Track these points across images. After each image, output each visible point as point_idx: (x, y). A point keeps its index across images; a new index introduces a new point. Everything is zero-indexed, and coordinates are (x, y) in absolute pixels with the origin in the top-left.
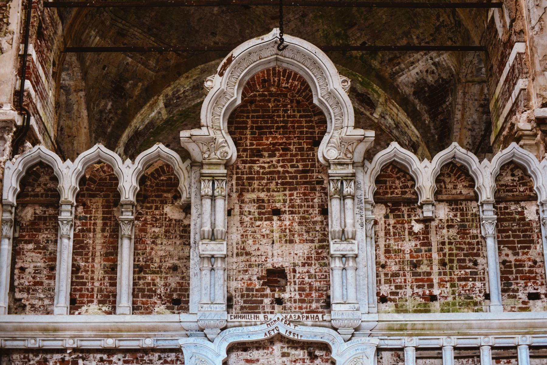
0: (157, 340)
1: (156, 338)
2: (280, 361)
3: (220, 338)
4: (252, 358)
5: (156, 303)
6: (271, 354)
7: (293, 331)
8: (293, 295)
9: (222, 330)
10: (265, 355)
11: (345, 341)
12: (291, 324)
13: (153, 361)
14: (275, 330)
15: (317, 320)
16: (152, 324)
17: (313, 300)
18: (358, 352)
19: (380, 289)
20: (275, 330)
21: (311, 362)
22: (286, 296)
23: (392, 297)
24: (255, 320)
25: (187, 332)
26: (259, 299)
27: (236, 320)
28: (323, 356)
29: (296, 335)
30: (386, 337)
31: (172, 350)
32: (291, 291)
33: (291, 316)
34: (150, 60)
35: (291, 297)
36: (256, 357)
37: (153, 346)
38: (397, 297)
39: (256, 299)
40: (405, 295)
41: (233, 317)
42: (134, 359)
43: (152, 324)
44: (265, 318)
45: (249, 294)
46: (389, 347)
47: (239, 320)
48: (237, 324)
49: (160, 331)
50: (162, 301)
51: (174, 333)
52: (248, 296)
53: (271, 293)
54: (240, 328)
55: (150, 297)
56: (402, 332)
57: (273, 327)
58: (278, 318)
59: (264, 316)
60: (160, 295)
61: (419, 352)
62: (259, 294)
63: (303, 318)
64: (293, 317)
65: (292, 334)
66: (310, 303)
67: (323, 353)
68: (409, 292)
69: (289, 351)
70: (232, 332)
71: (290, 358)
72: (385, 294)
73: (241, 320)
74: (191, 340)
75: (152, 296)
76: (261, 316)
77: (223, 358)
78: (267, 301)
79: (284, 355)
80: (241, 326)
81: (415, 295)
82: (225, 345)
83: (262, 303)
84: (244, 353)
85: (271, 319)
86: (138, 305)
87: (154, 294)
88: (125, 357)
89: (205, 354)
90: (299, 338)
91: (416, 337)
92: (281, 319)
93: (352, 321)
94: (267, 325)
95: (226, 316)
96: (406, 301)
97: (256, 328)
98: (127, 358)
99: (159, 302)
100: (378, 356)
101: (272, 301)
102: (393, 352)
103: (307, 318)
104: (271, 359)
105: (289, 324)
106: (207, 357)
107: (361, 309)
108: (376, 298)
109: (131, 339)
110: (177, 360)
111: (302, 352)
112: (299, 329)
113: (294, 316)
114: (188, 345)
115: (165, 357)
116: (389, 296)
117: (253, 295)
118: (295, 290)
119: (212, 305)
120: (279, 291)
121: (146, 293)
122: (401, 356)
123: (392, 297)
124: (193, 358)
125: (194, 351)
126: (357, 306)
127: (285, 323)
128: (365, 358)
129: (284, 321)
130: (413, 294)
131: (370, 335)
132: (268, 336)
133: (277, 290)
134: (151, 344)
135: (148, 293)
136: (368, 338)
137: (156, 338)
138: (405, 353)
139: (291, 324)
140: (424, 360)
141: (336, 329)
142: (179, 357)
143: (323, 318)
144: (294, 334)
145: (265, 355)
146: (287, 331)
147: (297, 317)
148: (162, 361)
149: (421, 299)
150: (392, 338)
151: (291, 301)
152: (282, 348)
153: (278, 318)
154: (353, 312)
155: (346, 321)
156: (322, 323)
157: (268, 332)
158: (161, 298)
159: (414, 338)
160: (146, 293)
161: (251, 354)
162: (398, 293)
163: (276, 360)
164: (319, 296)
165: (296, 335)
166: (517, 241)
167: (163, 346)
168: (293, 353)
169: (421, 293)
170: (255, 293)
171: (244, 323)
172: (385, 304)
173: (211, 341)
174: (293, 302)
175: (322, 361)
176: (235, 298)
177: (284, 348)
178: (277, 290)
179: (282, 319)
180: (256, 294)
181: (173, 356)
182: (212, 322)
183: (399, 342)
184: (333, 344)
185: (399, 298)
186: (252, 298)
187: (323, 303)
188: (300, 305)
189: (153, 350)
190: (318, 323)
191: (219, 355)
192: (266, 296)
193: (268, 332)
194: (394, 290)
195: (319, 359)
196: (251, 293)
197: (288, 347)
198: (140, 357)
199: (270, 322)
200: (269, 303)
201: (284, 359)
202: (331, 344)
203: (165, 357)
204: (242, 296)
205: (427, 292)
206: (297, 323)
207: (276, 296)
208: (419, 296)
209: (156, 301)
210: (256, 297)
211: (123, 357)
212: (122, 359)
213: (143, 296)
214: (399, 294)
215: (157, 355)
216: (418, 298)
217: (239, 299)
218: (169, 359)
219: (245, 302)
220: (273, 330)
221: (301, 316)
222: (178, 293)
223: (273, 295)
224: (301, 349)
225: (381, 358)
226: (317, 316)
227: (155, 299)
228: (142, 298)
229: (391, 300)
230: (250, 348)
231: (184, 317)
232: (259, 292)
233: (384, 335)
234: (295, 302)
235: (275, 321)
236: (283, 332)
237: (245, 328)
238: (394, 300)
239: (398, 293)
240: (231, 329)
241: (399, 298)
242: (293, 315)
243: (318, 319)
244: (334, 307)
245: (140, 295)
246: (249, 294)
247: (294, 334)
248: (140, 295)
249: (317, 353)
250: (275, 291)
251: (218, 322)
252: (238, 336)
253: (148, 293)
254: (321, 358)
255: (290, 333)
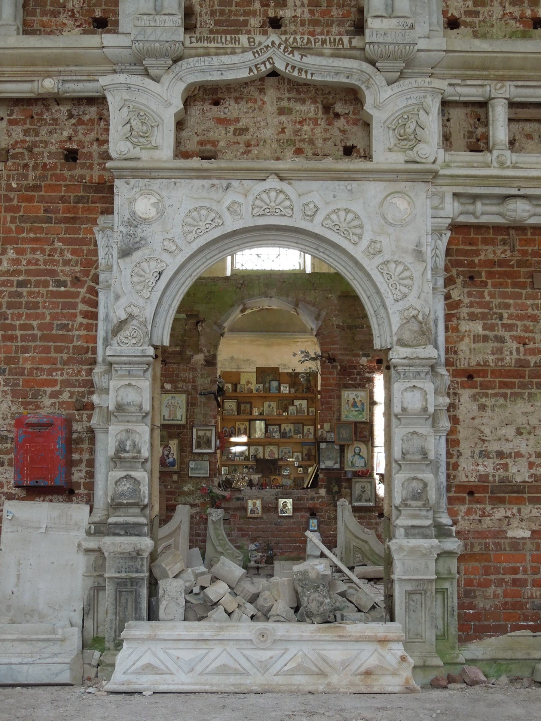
0: (64, 81)
1: (61, 78)
2: (276, 121)
3: (171, 75)
4: (229, 116)
5: (65, 24)
6: (260, 109)
7: (297, 64)
8: (299, 12)
9: (175, 61)
10: (251, 111)
11: (390, 83)
12: (296, 53)
13: (60, 121)
14: (267, 63)
15: (340, 46)
16: (54, 51)
17: (333, 22)
18: (410, 102)
19: (448, 6)
20: (267, 63)
21: (329, 124)
22: (287, 13)
23: (468, 19)
24: (234, 46)
25: (115, 67)
26: (241, 18)
27: (199, 45)
28: (348, 114)
29: (303, 73)
30: (459, 82)
31: (91, 101)
32: (295, 6)
33: (295, 39)
34: (251, 391)
35: (295, 16)
36: (235, 115)
37: (56, 90)
38: (476, 20)
39: (235, 18)
40: (491, 16)
41: (194, 40)
42: (26, 117)
43: (54, 51)
44: (249, 42)
45: (224, 10)
46: (462, 99)
47: (206, 44)
48: (201, 51)
49: (68, 65)
50: (76, 20)
51: (93, 68)
52: (222, 13)
53: (262, 9)
54: (206, 58)
55: (55, 14)
56: (486, 73)
57: (264, 57)
58: (273, 43)
59: (249, 39)
60: (72, 11)
61: (514, 110)
62: (241, 9)
63: (315, 43)
64: (299, 40)
65: (296, 69)
66: (328, 25)
67: (348, 109)
68: (497, 11)
69: (291, 105)
70: (192, 64)
71: (292, 117)
72: (456, 15)
73: (210, 45)
74: (122, 78)
75: (59, 13)
76: (244, 39)
77: (176, 110)
78: (254, 22)
79: (282, 111)
80: (208, 55)
81: (507, 17)
82: (181, 87)
83: (247, 26)
84: (215, 108)
85: (260, 44)
86: (35, 28)
87: (61, 10)
88: (11, 115)
89: (144, 101)
90: (309, 77)
91: (510, 83)
92: (277, 43)
93: (401, 47)
94: (254, 53)
95: (180, 35)
96: (492, 26)
97: (235, 59)
98: (14, 117)
99: (70, 22)
100: (443, 115)
101: (264, 21)
102: (469, 110)
103: (324, 42)
104: (259, 119)
105: (292, 52)
106: (148, 107)
107: (417, 28)
108: (442, 20)
109: (19, 79)
110: (101, 119)
111: (313, 108)
112: (310, 60)
113: (301, 40)
114: (117, 87)
115: (79, 115)
116: (463, 18)
117: (230, 11)
118: (303, 5)
119: (157, 17)
120: (275, 6)
121: (48, 8)
122: (483, 117)
123: (468, 19)
124: (125, 110)
125: (126, 97)
126: (410, 22)
127: (284, 51)
128: (422, 112)
129: (282, 47)
130: (504, 15)
131: (431, 75)
132: (256, 72)
133: (272, 4)
134: (53, 88)
135: (52, 8)
136: (429, 79)
137: (61, 78)
138: (490, 110)
139: (296, 53)
140: (521, 124)
141: (373, 63)
142: (103, 114)
143: (350, 42)
144: (300, 70)
145: (251, 111)
146: (287, 65)
147: (305, 41)
148: (73, 121)
149: (518, 24)
150: (469, 82)
151: (295, 22)
152: (280, 99)
153: (273, 43)
154: (403, 32)
155: (392, 47)
156: (349, 52)
157: (256, 66)
158: (73, 16)
159: (508, 83)
160: (48, 8)
161: (226, 110)
162: (479, 12)
163: (269, 120)
164: (344, 16)
165: (303, 73)
166: (512, 282)
167: (74, 91)
168: (298, 108)
169: (517, 14)
170: (233, 8)
171: (213, 51)
172: (455, 31)
173: (157, 79)
174: (298, 24)
175: (348, 122)
176: (201, 16)
177: (283, 99)
178: (272, 4)
179: (280, 45)
180: (237, 10)
181: (92, 112)
182: (157, 44)
183: (480, 91)
184: (368, 88)
185: (480, 22)
186: (229, 16)
187: (349, 26)
188: (312, 29)
189: (58, 100)
190: (342, 52)
191: (170, 104)
192: (254, 13)
193: (256, 66)
194: (471, 8)
195: (342, 118)
196: (227, 9)
197: (289, 99)
198: (38, 114)
199: (258, 49)
200: (258, 25)
201: (283, 118)
202: (363, 87)
203: (79, 115)
204: (213, 13)
205: (528, 13)
206: (305, 50)
207: (271, 14)
208: (515, 19)
209: (65, 21)
210: (236, 15)
211: (8, 115)
212: (6, 118)
213: (44, 13)
214: (481, 15)
215: (64, 109)
216: (512, 22)
217: (206, 18)
218: (86, 118)
219: (217, 23)
220: (264, 63)
221: (312, 39)
222: (103, 7)
223: (266, 12)
224: (311, 103)
225: (448, 120)
226: (341, 39)
227: (63, 18)
228: (42, 16)
229: (466, 24)
230: (224, 99)
231: (108, 39)
232: (241, 6)
233: (455, 77)
234: (303, 24)
235: (267, 47)
236: (280, 66)
237: (215, 58)
238: (471, 25)
239: (479, 12)
240: (190, 60)
241: (480, 22)
242: (298, 37)
243: (343, 44)
244: (372, 24)
245: (38, 10)
246: (224, 10)
247: (300, 70)
248: (38, 10)
249: (339, 108)
250: (268, 5)
251: (167, 45)
252: (203, 71)
253: (52, 8)
254: (345, 118)
255: (293, 68)
